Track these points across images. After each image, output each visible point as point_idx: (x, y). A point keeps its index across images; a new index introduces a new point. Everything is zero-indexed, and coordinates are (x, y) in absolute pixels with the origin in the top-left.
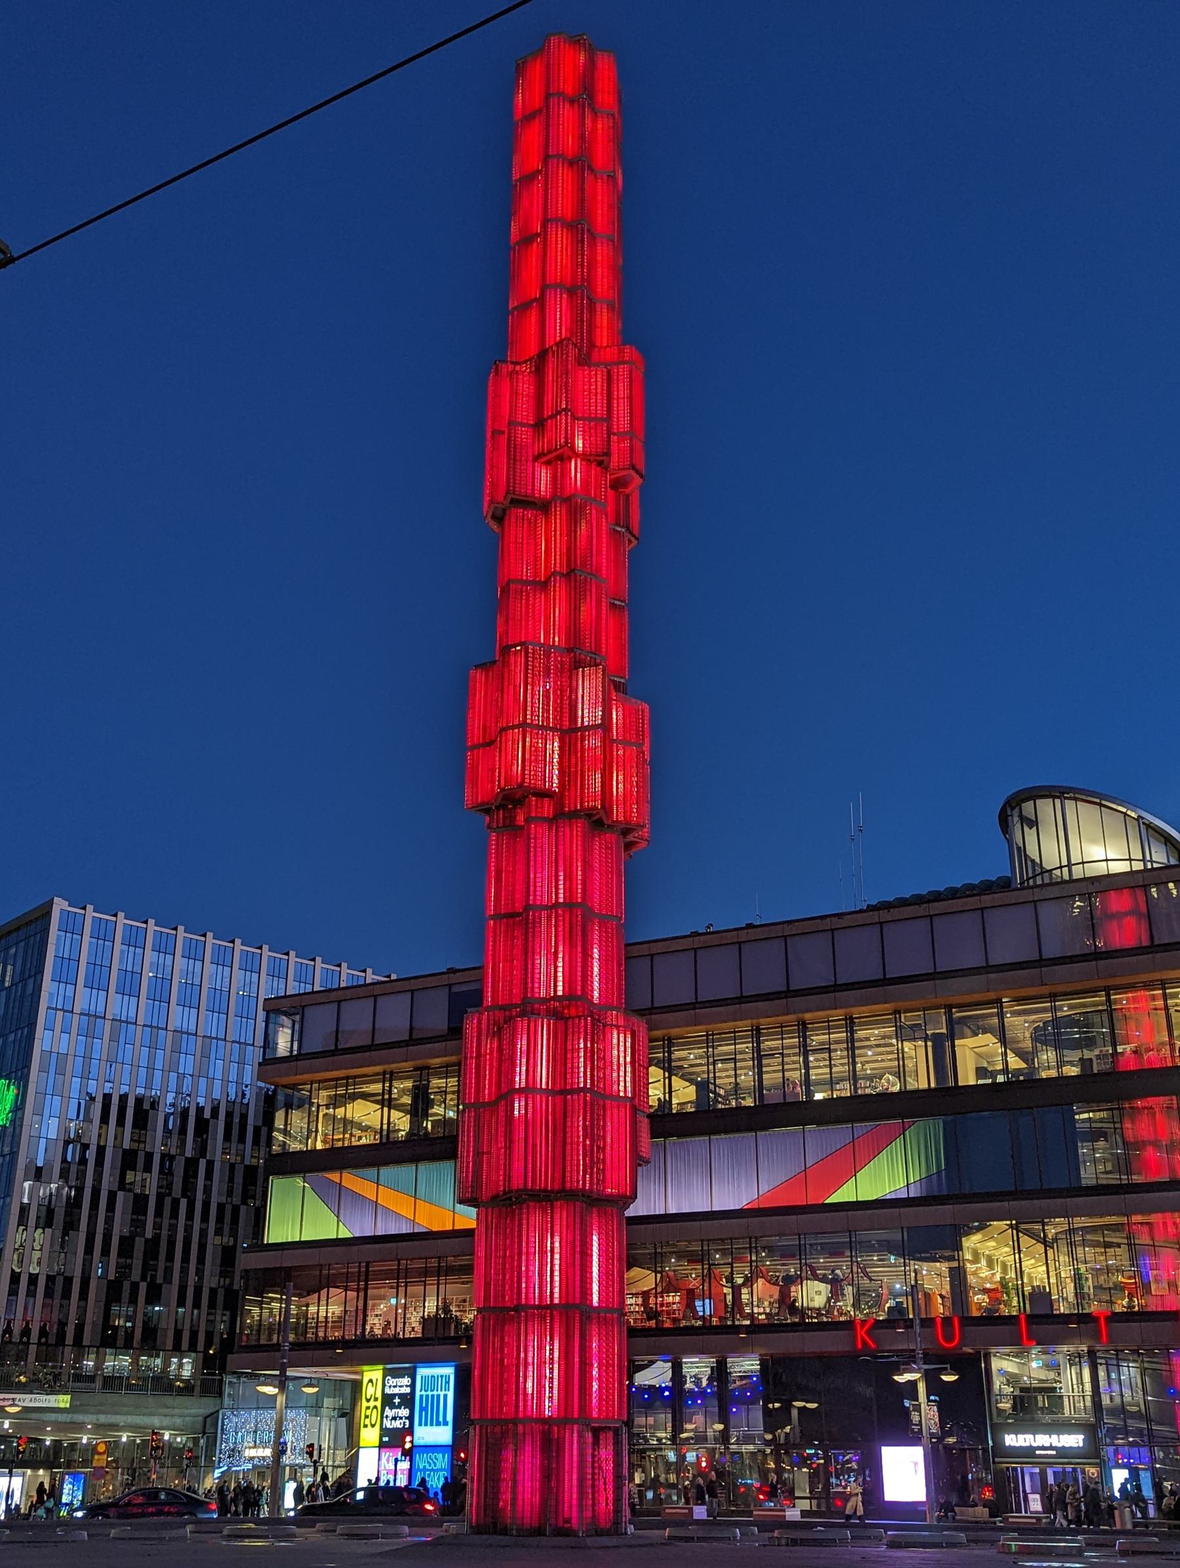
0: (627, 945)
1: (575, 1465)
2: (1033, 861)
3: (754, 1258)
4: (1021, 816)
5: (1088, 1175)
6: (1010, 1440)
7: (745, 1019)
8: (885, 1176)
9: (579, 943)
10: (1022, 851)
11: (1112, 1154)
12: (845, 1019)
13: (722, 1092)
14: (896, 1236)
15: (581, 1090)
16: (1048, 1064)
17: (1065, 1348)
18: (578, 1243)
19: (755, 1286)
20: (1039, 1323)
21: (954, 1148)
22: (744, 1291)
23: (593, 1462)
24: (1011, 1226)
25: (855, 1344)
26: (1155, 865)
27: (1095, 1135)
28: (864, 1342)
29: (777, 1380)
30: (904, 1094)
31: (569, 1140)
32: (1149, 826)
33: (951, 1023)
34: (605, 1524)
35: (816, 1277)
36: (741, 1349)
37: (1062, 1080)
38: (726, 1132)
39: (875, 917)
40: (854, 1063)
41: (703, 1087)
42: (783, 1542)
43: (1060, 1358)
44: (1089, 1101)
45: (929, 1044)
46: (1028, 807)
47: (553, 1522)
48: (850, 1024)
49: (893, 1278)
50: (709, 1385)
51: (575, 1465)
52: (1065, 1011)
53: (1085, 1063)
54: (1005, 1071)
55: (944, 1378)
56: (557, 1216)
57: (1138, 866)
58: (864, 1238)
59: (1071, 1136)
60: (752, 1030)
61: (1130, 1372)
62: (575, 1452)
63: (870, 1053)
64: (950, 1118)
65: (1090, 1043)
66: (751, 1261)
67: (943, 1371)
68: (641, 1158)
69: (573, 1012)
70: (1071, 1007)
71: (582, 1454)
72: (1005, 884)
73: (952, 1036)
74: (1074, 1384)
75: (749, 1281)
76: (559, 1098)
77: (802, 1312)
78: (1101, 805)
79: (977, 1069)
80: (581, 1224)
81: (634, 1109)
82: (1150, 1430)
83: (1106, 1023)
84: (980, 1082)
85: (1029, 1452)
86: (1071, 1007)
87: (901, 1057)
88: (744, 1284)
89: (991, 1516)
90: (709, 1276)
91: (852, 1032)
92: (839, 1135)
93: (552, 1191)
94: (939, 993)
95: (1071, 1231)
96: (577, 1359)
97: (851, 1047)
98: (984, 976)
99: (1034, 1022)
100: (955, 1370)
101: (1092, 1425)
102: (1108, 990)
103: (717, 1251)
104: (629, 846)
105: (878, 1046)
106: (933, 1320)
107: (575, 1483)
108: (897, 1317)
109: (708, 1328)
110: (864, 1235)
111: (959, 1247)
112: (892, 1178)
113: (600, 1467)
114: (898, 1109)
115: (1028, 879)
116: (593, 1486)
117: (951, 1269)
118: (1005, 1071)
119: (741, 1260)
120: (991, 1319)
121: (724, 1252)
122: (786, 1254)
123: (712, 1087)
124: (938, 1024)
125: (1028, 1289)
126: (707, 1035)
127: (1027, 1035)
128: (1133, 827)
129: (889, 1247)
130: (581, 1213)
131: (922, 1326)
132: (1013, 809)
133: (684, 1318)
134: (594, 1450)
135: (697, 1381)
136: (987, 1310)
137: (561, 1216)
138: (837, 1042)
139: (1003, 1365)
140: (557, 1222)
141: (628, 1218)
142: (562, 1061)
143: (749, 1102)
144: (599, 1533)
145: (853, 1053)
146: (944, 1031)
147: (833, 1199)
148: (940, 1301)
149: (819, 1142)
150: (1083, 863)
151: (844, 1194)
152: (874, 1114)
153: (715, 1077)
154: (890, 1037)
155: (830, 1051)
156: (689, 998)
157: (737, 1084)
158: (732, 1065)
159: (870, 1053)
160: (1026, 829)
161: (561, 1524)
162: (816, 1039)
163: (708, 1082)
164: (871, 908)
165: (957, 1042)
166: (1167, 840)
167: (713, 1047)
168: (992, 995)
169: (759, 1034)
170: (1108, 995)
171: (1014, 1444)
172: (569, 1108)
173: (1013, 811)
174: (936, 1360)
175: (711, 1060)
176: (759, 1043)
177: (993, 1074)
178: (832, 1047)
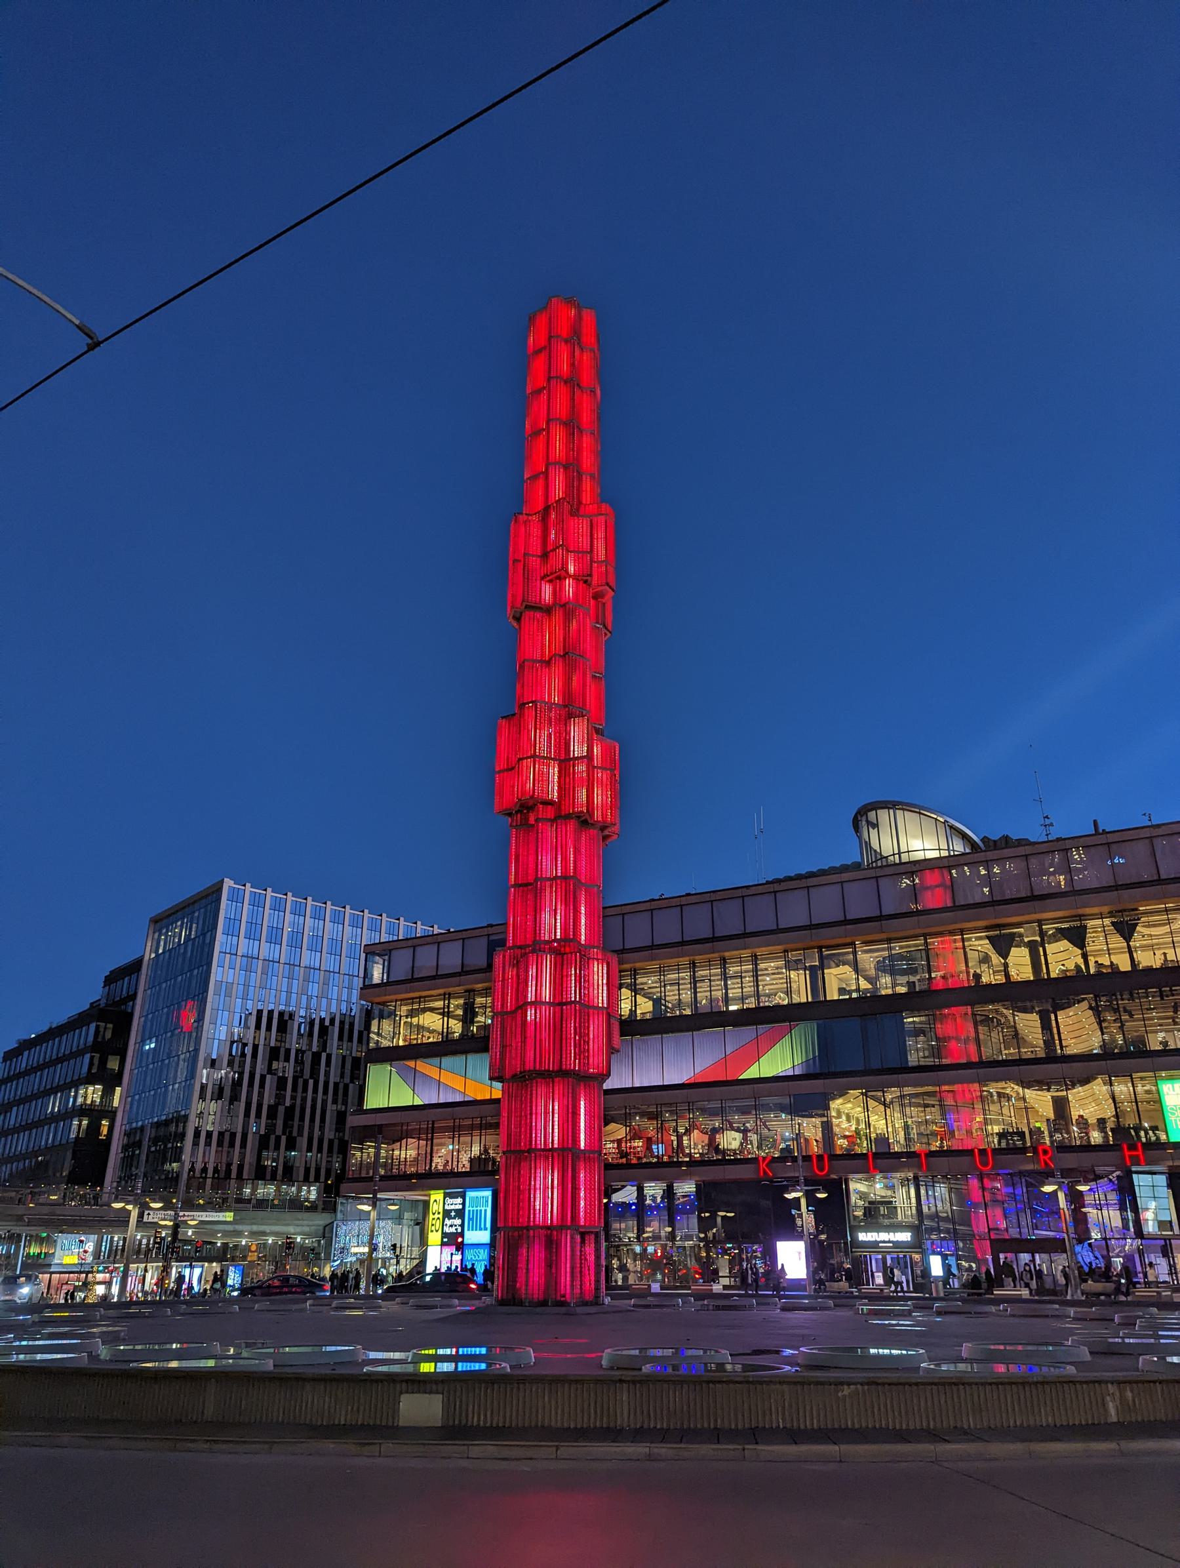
0: (604, 908)
5: (913, 1059)
8: (780, 1060)
10: (868, 844)
16: (886, 985)
17: (898, 1175)
20: (881, 1158)
22: (685, 1138)
28: (765, 1172)
29: (707, 1197)
30: (791, 1006)
32: (951, 827)
33: (821, 958)
34: (589, 1297)
35: (733, 1129)
36: (682, 1177)
37: (895, 996)
38: (672, 1032)
39: (771, 888)
40: (758, 986)
41: (657, 1002)
46: (872, 815)
48: (755, 959)
49: (784, 1129)
52: (897, 951)
53: (911, 985)
56: (556, 1088)
57: (945, 854)
61: (941, 1190)
72: (857, 866)
73: (822, 967)
74: (904, 1199)
75: (688, 1132)
76: (558, 1008)
77: (724, 1152)
81: (609, 1016)
82: (955, 1229)
85: (875, 1244)
86: (901, 947)
87: (789, 981)
90: (661, 1129)
91: (756, 965)
92: (748, 1033)
94: (820, 940)
95: (902, 1097)
100: (825, 1190)
102: (925, 936)
106: (810, 1157)
108: (787, 1156)
109: (660, 1164)
111: (828, 1108)
112: (783, 1060)
117: (822, 1122)
118: (858, 990)
120: (850, 1156)
121: (671, 1112)
122: (712, 1113)
125: (873, 1136)
129: (782, 1108)
135: (654, 1199)
136: (846, 1149)
140: (556, 1092)
143: (688, 1012)
144: (585, 1304)
149: (737, 1038)
151: (751, 1073)
152: (769, 1019)
162: (732, 970)
164: (768, 883)
166: (964, 836)
168: (848, 940)
169: (694, 966)
170: (925, 939)
173: (862, 818)
174: (812, 1183)
177: (850, 992)
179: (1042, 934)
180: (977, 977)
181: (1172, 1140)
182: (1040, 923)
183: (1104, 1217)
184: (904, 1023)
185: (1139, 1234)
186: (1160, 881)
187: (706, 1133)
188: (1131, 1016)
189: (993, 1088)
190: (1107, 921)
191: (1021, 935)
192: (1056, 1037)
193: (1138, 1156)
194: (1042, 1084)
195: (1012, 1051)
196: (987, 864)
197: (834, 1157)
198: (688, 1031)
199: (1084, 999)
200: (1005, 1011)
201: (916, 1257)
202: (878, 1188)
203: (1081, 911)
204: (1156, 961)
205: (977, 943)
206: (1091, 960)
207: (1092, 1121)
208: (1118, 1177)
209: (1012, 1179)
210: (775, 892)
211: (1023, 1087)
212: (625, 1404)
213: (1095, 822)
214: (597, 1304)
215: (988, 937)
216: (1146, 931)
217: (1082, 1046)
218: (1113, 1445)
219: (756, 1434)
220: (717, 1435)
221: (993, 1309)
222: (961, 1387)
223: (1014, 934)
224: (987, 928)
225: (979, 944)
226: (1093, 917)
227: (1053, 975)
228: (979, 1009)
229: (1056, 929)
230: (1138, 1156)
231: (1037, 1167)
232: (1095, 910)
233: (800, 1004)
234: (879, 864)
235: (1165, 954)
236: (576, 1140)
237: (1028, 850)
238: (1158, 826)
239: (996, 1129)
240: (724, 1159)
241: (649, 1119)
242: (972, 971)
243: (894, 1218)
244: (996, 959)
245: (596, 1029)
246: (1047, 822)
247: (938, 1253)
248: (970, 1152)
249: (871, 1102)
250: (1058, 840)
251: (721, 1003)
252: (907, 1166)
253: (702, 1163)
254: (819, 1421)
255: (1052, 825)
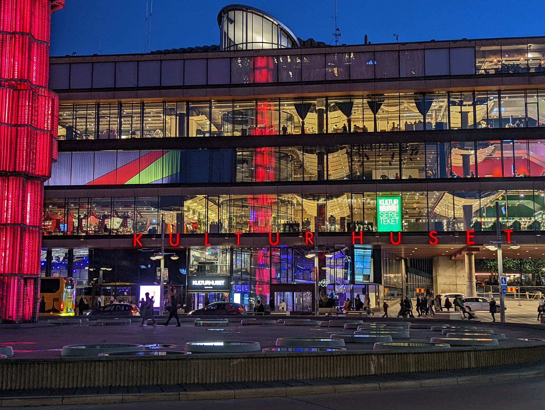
0: (50, 58)
1: (15, 294)
2: (230, 39)
3: (89, 207)
4: (228, 18)
5: (239, 177)
6: (195, 283)
7: (94, 99)
8: (153, 174)
9: (27, 53)
10: (226, 34)
11: (250, 170)
12: (141, 103)
13: (79, 132)
14: (156, 199)
15: (26, 125)
16: (228, 130)
17: (221, 247)
18: (21, 196)
19: (89, 219)
20: (214, 236)
21: (185, 163)
22: (84, 221)
23: (24, 292)
24: (205, 197)
25: (133, 244)
26: (282, 47)
27: (243, 161)
28: (137, 243)
29: (96, 258)
30: (165, 139)
31: (18, 149)
32: (282, 29)
33: (188, 109)
34: (27, 318)
35: (118, 217)
36: (79, 246)
37: (233, 138)
38: (80, 150)
39: (159, 57)
40: (143, 123)
41: (70, 129)
42: (102, 324)
43: (218, 251)
44: (243, 147)
45: (178, 117)
46: (231, 14)
47: (4, 317)
48: (143, 106)
49: (153, 218)
50: (63, 260)
51: (15, 294)
52: (238, 108)
53: (243, 131)
54: (210, 132)
55: (172, 258)
56: (11, 183)
57: (275, 47)
58: (141, 200)
59: (235, 161)
60: (96, 105)
61: (246, 256)
62: (16, 288)
63: (150, 119)
64: (183, 151)
65: (246, 122)
66: (88, 208)
67: (327, 253)
68: (53, 159)
69: (22, 87)
70: (240, 106)
71: (19, 289)
72: (215, 49)
73: (188, 115)
74: (223, 260)
75: (86, 217)
76: (14, 129)
77: (110, 231)
78: (263, 17)
79: (197, 130)
80: (23, 187)
81: (52, 136)
82: (251, 279)
83: (254, 115)
84: (198, 136)
85: (202, 287)
86: (240, 106)
87: (165, 122)
88: (84, 218)
89: (185, 312)
90: (67, 214)
91: (143, 109)
92: (134, 155)
93: (9, 172)
94: (185, 95)
95: (230, 200)
96: (18, 248)
97: (142, 115)
98: (158, 91)
99: (223, 111)
100: (177, 255)
101: (229, 277)
102: (257, 100)
103: (72, 203)
104: (53, 7)
105: (154, 116)
106: (168, 235)
107: (15, 301)
108: (152, 234)
109: (65, 237)
110: (140, 199)
111: (182, 205)
112: (156, 175)
113: (27, 294)
114: (162, 145)
115: (228, 47)
116: (23, 302)
117: (177, 214)
118: (210, 132)
119: (82, 207)
120: (193, 235)
121: (75, 204)
122: (104, 206)
123: (74, 130)
124: (182, 109)
125: (209, 223)
126: (74, 105)
127: (220, 117)
128: (275, 29)
129: (152, 204)
130: (23, 182)
131: (165, 237)
132: (225, 14)
133: (54, 232)
134: (24, 287)
135: (58, 258)
136: (192, 231)
137: (13, 183)
138: (135, 113)
139: (195, 253)
140: (11, 186)
141: (45, 186)
142: (16, 110)
143: (91, 138)
144: (25, 322)
145: (143, 119)
146: (185, 112)
147: (128, 182)
148: (171, 227)
149: (124, 158)
150: (252, 42)
151: (134, 181)
152: (148, 146)
153: (76, 125)
154: (160, 113)
155: (132, 117)
156: (110, 85)
157: (87, 129)
158: (85, 120)
159: (150, 119)
160: (229, 24)
161: (7, 318)
162: (126, 111)
163: (73, 127)
164: (152, 53)
165: (190, 118)
166: (289, 36)
167: (76, 111)
168: (208, 98)
169: (99, 107)
170: (257, 102)
171: (196, 284)
172: (19, 134)
173: (224, 15)
174: (169, 251)
175: (75, 117)
176: (98, 111)
177: (204, 133)
178: (88, 116)
179: (327, 105)
180: (285, 129)
181: (379, 231)
182: (327, 98)
183: (335, 272)
184: (236, 155)
185: (353, 281)
186: (399, 79)
187: (100, 218)
188: (368, 159)
189: (285, 197)
190: (365, 101)
191: (315, 105)
192: (325, 169)
193: (359, 239)
194: (315, 197)
195: (299, 176)
196: (301, 57)
197: (182, 235)
198: (91, 150)
199: (345, 147)
200: (298, 151)
201: (226, 294)
202: (207, 254)
203: (352, 93)
204: (388, 128)
205: (287, 108)
206: (352, 125)
207: (338, 218)
208: (346, 250)
209: (284, 251)
210: (161, 60)
211: (303, 198)
212: (101, 374)
213: (366, 36)
214: (33, 322)
215: (295, 105)
216: (386, 109)
217: (339, 175)
218: (376, 385)
219: (183, 387)
220: (161, 388)
221: (275, 322)
222: (298, 359)
223: (311, 104)
224: (295, 99)
225: (289, 108)
226: (358, 97)
227: (329, 132)
228: (283, 149)
229: (336, 103)
230: (359, 239)
231: (303, 244)
232: (360, 93)
233: (170, 138)
234: (232, 49)
235: (394, 123)
236: (24, 218)
237: (328, 50)
238: (404, 44)
239: (283, 222)
240: (111, 235)
241: (58, 207)
242: (282, 126)
243: (214, 271)
244: (297, 118)
245: (41, 145)
246: (338, 33)
247: (238, 292)
248: (267, 234)
249: (209, 202)
250: (344, 45)
251: (116, 134)
252: (229, 242)
253: (95, 237)
254: (218, 379)
255: (340, 35)
